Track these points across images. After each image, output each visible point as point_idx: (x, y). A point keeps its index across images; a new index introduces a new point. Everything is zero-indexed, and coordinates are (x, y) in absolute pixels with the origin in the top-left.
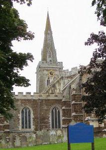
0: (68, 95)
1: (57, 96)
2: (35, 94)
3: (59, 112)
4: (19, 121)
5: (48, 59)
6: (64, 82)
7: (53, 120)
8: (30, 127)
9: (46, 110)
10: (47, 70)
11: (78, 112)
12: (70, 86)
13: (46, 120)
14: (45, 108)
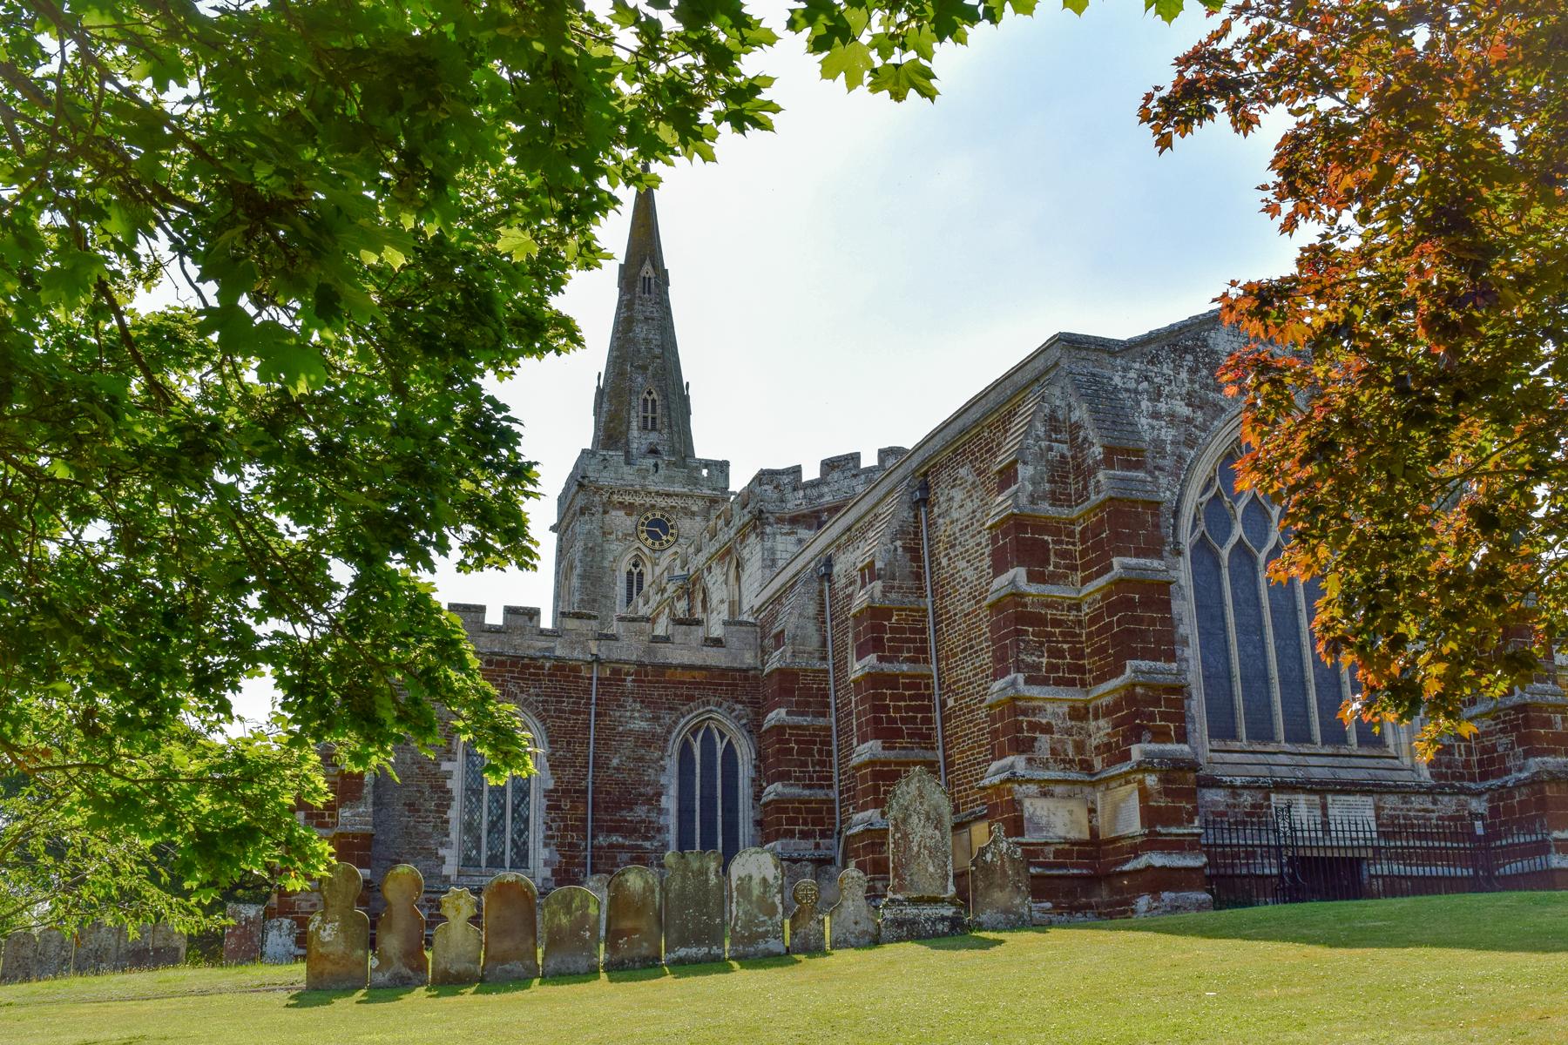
0: (811, 628)
1: (718, 642)
2: (571, 624)
3: (730, 751)
4: (443, 806)
5: (638, 439)
6: (773, 551)
7: (685, 812)
8: (521, 860)
9: (646, 740)
10: (630, 509)
11: (898, 733)
12: (829, 563)
13: (641, 811)
14: (640, 725)
